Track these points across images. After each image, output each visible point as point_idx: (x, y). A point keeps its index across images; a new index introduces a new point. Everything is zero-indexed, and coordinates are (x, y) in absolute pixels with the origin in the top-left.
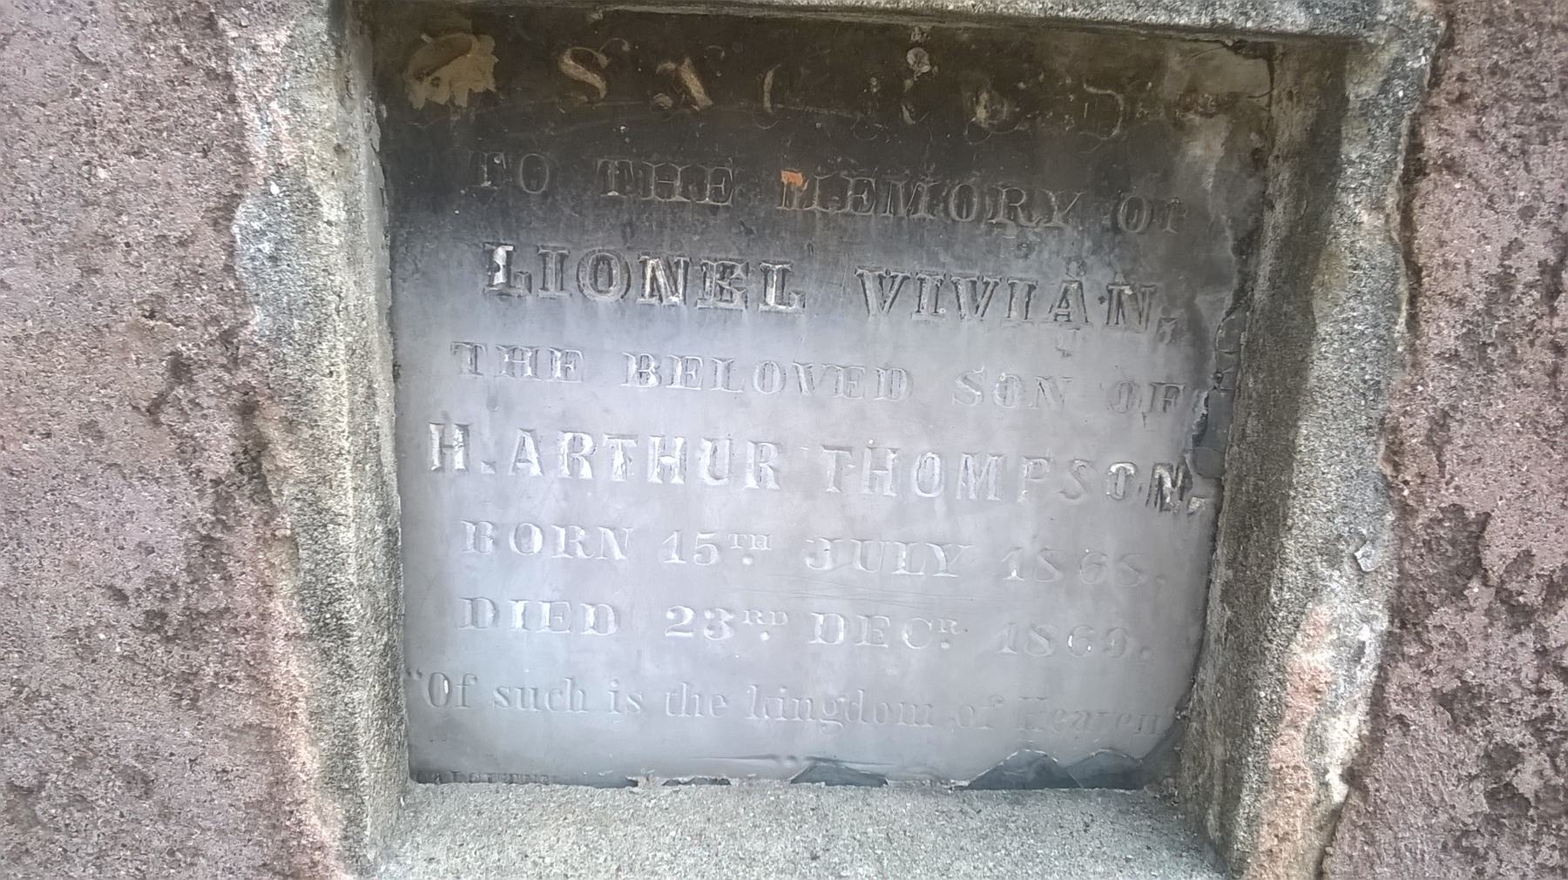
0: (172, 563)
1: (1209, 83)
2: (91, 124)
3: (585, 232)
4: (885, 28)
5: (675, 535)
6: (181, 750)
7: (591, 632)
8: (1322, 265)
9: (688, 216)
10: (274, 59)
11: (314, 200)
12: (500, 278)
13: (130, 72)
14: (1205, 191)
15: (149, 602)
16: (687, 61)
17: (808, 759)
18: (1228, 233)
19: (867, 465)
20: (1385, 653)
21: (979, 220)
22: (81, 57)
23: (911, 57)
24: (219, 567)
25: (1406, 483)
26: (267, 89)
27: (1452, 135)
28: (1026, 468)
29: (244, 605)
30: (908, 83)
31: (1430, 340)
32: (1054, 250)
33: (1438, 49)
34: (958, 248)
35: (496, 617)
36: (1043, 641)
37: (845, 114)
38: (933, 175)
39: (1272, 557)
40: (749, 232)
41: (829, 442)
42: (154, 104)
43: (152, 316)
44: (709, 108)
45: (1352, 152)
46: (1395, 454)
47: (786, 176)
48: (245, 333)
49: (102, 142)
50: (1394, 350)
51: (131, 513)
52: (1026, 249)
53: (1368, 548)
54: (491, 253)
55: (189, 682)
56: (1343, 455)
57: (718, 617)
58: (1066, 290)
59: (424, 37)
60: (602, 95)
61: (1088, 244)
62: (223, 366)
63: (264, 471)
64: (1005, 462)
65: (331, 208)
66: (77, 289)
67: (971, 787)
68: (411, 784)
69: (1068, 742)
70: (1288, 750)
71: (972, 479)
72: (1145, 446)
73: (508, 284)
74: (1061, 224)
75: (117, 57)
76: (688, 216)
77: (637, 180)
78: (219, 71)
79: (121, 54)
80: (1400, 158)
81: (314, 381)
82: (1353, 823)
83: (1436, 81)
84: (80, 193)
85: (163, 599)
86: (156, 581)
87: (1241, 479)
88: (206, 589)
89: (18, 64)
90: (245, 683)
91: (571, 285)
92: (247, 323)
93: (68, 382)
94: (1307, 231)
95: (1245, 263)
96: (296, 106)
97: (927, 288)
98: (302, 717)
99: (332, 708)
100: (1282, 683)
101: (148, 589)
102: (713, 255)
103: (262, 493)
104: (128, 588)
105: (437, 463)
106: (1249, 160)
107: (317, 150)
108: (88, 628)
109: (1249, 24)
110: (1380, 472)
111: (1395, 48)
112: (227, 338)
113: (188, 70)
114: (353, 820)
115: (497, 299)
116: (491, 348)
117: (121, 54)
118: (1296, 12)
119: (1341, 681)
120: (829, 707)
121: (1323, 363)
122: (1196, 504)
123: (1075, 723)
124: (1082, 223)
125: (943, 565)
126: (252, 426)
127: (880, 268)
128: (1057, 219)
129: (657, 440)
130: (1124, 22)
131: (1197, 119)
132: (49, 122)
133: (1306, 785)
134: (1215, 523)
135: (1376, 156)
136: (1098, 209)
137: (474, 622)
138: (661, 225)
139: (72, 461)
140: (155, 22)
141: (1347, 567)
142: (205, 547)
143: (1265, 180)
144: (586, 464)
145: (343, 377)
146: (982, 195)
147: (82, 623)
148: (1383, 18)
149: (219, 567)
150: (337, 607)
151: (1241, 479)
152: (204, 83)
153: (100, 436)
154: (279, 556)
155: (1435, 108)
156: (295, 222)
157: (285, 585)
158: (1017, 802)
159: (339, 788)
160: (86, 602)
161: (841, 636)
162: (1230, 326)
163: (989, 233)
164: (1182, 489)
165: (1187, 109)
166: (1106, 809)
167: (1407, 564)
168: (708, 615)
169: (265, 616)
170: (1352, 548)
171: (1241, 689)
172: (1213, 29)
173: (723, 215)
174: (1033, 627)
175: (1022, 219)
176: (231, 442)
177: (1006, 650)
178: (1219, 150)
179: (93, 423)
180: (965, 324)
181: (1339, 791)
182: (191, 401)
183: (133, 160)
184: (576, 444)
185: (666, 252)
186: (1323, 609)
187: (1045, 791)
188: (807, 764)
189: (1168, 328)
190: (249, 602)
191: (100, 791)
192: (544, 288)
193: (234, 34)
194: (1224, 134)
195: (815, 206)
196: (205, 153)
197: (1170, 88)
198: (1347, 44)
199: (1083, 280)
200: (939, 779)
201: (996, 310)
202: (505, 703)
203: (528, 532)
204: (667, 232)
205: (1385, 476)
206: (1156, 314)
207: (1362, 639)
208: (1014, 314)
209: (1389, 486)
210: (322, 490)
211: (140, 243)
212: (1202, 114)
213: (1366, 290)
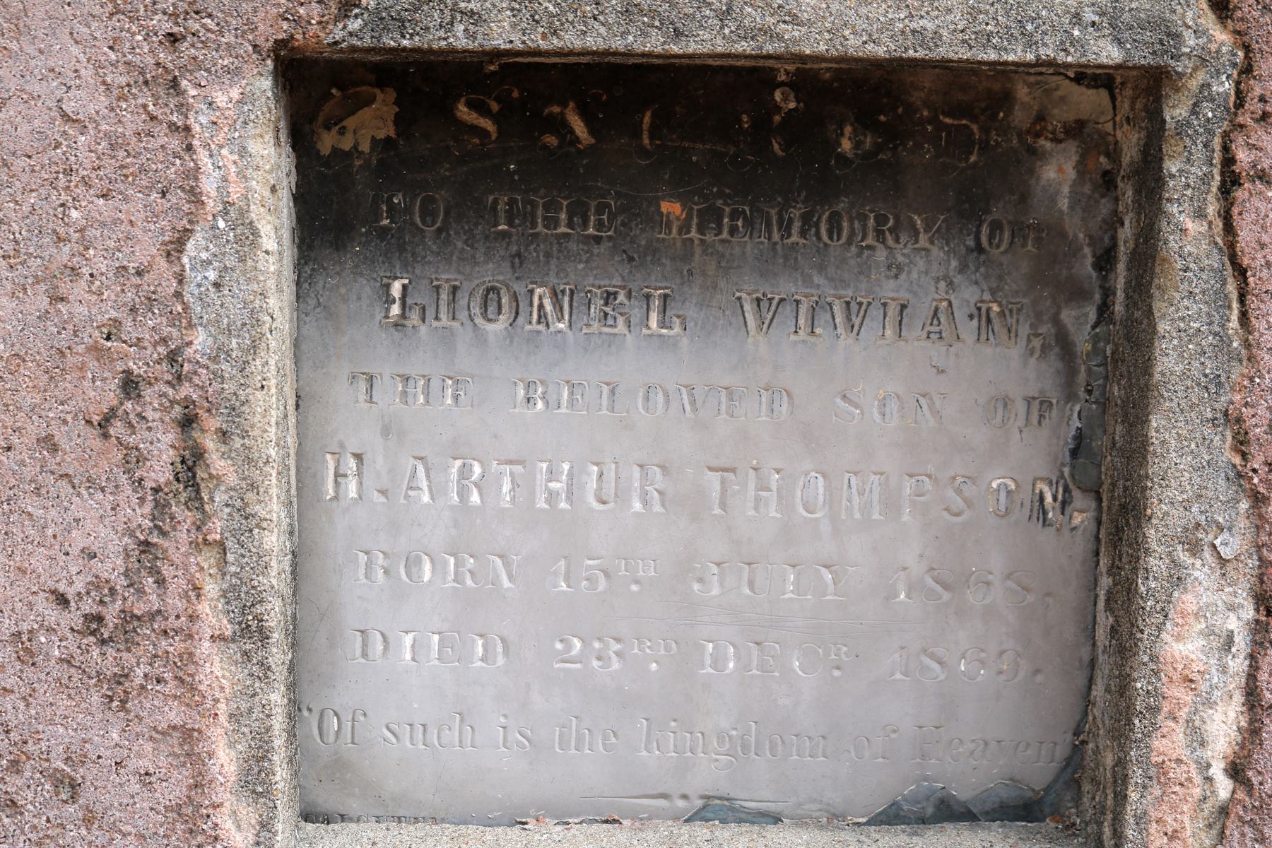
0: (111, 568)
1: (1056, 111)
2: (69, 172)
3: (476, 264)
4: (754, 70)
5: (562, 563)
6: (108, 753)
7: (479, 664)
8: (1158, 270)
9: (573, 246)
10: (227, 113)
11: (255, 233)
12: (395, 310)
13: (104, 127)
14: (1061, 211)
15: (89, 606)
16: (572, 105)
17: (702, 797)
18: (1087, 250)
19: (752, 486)
20: (1254, 642)
21: (849, 242)
22: (66, 118)
23: (778, 96)
24: (154, 571)
25: (1255, 471)
26: (220, 138)
27: (1261, 149)
28: (908, 486)
29: (175, 607)
30: (777, 118)
31: (1262, 335)
32: (922, 270)
33: (1239, 75)
34: (831, 270)
35: (386, 649)
36: (935, 666)
37: (719, 148)
38: (803, 202)
39: (1138, 548)
40: (631, 259)
41: (715, 464)
42: (122, 154)
43: (108, 338)
44: (591, 146)
45: (1171, 166)
46: (1241, 444)
47: (665, 207)
48: (189, 352)
49: (76, 186)
50: (1229, 345)
51: (77, 521)
52: (895, 270)
53: (1226, 535)
54: (388, 286)
55: (119, 683)
56: (1193, 446)
57: (607, 647)
58: (937, 309)
59: (334, 91)
60: (494, 136)
61: (954, 263)
62: (168, 382)
63: (198, 480)
64: (887, 479)
65: (268, 242)
66: (43, 317)
67: (868, 823)
68: (303, 824)
69: (969, 776)
70: (1169, 743)
71: (856, 499)
72: (1024, 459)
73: (403, 316)
74: (927, 245)
75: (94, 115)
76: (573, 246)
77: (525, 213)
78: (180, 124)
79: (97, 112)
80: (1216, 172)
81: (247, 395)
82: (1240, 818)
83: (1240, 101)
84: (54, 231)
85: (101, 602)
86: (96, 584)
87: (1114, 485)
88: (141, 592)
89: (11, 123)
90: (172, 684)
91: (463, 315)
92: (191, 343)
93: (28, 399)
94: (1146, 242)
95: (1105, 278)
96: (243, 153)
97: (803, 309)
98: (223, 718)
99: (250, 711)
100: (1156, 673)
101: (88, 593)
102: (597, 283)
103: (196, 501)
104: (70, 593)
105: (331, 492)
106: (1101, 181)
107: (259, 189)
108: (30, 632)
109: (1070, 59)
110: (1229, 462)
111: (1201, 76)
112: (172, 357)
113: (152, 124)
114: (265, 825)
115: (392, 330)
116: (386, 378)
117: (97, 112)
118: (1110, 48)
119: (1214, 670)
120: (721, 740)
121: (1165, 359)
122: (1078, 519)
123: (972, 753)
124: (947, 244)
125: (831, 588)
126: (190, 437)
127: (757, 291)
128: (923, 240)
129: (545, 466)
130: (960, 61)
131: (1049, 145)
132: (33, 171)
133: (1189, 780)
134: (1098, 539)
135: (1193, 170)
136: (961, 230)
137: (364, 654)
138: (548, 255)
139: (28, 472)
140: (128, 85)
141: (1207, 554)
142: (143, 552)
143: (1117, 200)
144: (475, 491)
145: (273, 391)
146: (851, 221)
147: (25, 627)
148: (1188, 50)
149: (154, 571)
150: (259, 609)
151: (1114, 485)
152: (166, 135)
153: (54, 448)
154: (207, 559)
155: (1241, 126)
156: (237, 252)
157: (211, 588)
158: (916, 834)
159: (254, 791)
160: (30, 606)
161: (731, 665)
162: (1095, 339)
163: (859, 255)
164: (1064, 504)
165: (1038, 135)
166: (1007, 837)
167: (1265, 551)
168: (597, 645)
169: (193, 618)
170: (1211, 537)
171: (1123, 687)
172: (1039, 63)
173: (605, 245)
174: (924, 651)
175: (890, 242)
176: (171, 452)
177: (898, 676)
178: (1071, 174)
179: (50, 437)
180: (842, 342)
181: (1224, 787)
182: (138, 415)
183: (101, 201)
184: (465, 471)
185: (553, 280)
186: (1189, 597)
187: (945, 824)
188: (699, 803)
189: (1037, 343)
190: (180, 604)
191: (30, 796)
192: (437, 318)
193: (193, 92)
194: (1075, 158)
195: (693, 234)
196: (164, 194)
197: (1020, 118)
198: (1162, 73)
199: (952, 298)
200: (835, 816)
201: (871, 328)
202: (394, 740)
203: (419, 561)
204: (554, 262)
205: (1234, 466)
206: (1024, 330)
207: (1231, 627)
208: (888, 332)
209: (1239, 475)
210: (250, 496)
211: (102, 274)
212: (1052, 140)
213: (1197, 291)
